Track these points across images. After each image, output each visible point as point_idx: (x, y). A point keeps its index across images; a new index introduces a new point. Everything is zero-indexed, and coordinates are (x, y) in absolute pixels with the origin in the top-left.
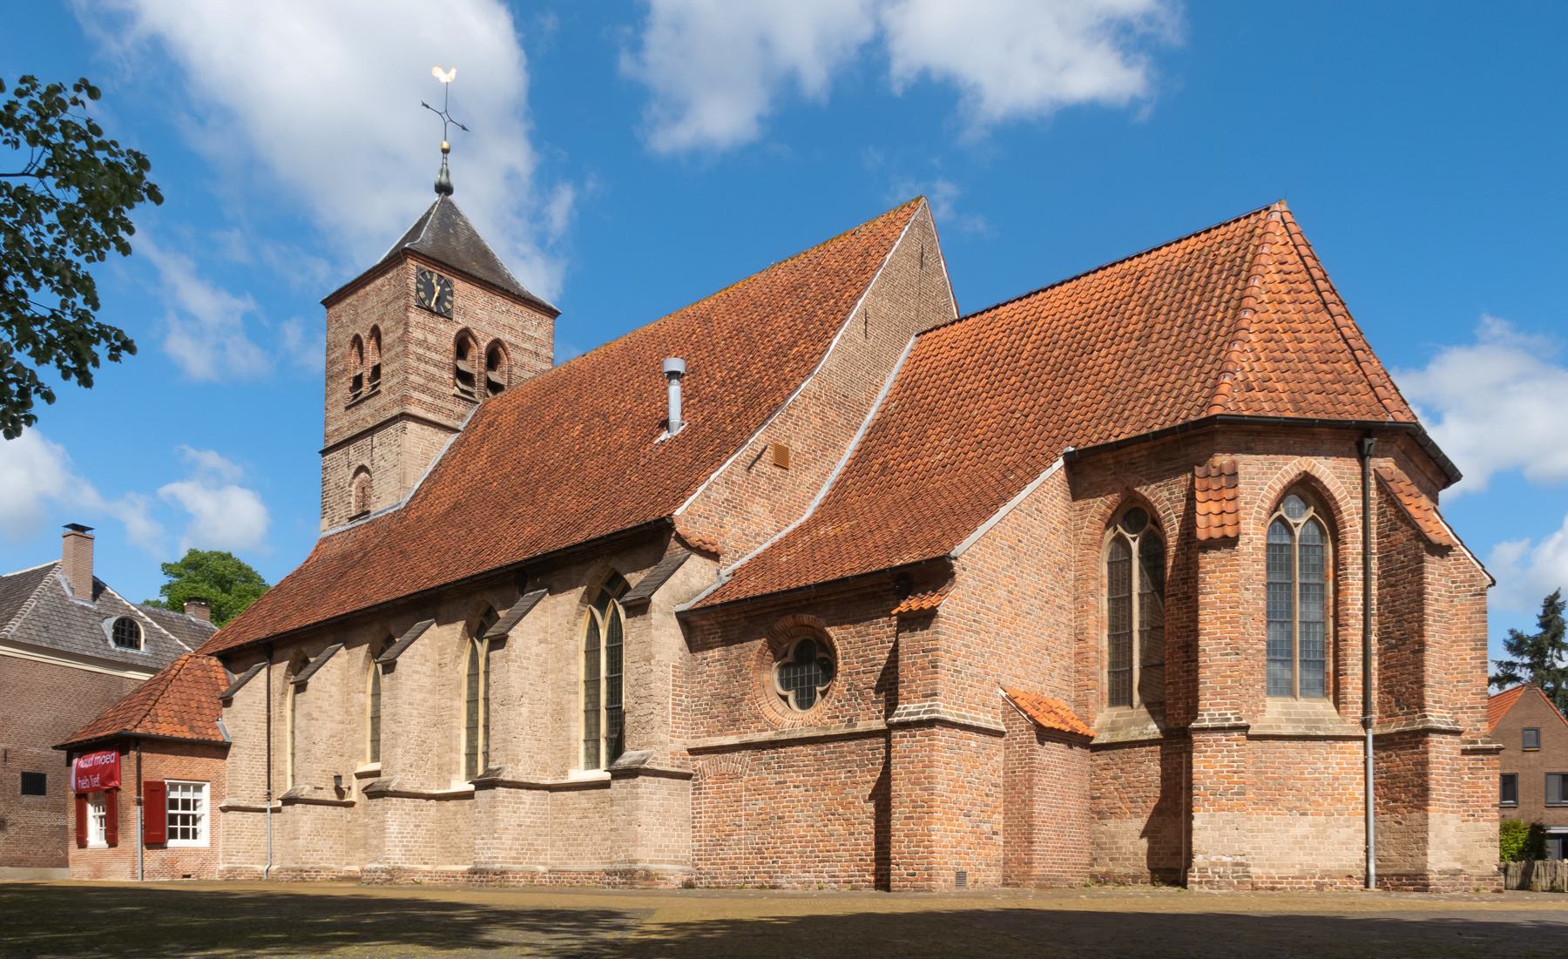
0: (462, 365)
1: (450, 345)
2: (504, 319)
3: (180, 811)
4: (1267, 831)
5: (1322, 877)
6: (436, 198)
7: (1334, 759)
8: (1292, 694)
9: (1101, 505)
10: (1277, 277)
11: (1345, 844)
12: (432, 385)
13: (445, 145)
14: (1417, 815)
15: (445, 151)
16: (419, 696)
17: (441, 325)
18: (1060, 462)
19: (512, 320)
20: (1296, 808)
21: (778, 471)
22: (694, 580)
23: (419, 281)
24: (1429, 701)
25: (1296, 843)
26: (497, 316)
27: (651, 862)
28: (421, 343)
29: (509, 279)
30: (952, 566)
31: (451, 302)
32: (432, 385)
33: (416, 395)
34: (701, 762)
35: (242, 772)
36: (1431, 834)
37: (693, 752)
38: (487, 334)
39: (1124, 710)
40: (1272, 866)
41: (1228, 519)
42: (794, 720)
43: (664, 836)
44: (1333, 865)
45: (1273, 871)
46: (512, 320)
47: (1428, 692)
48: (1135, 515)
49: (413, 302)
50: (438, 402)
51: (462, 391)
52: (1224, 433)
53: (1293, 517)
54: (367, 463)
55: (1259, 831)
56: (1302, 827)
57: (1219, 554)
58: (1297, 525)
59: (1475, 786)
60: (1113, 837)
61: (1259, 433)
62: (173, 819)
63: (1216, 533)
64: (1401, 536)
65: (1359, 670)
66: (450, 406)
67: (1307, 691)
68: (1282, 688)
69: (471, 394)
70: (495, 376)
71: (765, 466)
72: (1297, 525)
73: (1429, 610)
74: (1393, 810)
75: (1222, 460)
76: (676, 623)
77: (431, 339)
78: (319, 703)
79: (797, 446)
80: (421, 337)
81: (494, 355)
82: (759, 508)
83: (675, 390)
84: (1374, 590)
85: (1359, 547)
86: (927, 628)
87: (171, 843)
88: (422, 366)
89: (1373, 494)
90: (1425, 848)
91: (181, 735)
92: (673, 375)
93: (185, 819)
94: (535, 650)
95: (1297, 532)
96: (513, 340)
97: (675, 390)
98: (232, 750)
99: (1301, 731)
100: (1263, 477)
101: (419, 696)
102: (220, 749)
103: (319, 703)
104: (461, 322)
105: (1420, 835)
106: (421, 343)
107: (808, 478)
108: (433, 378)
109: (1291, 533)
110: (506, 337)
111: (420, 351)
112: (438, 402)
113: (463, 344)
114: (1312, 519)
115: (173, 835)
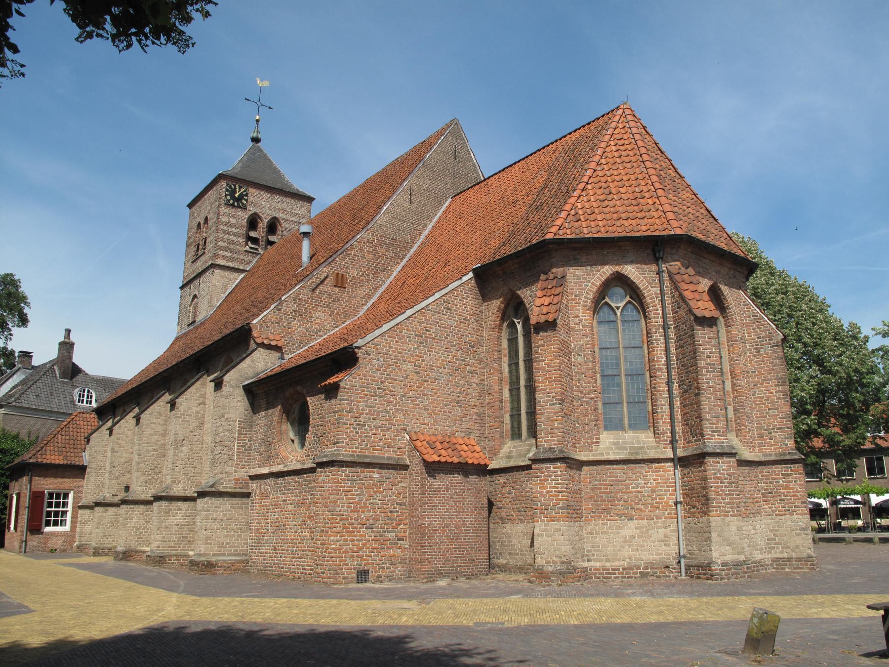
0: (253, 234)
1: (244, 223)
2: (279, 206)
3: (53, 509)
4: (603, 533)
5: (646, 568)
6: (251, 144)
7: (651, 476)
8: (622, 428)
9: (496, 304)
10: (614, 148)
11: (665, 541)
12: (232, 246)
13: (257, 117)
14: (704, 519)
15: (258, 121)
16: (154, 438)
17: (240, 213)
18: (471, 275)
19: (285, 206)
20: (624, 514)
21: (337, 290)
22: (258, 364)
23: (227, 190)
24: (708, 432)
25: (625, 542)
26: (274, 205)
27: (214, 555)
28: (226, 224)
29: (287, 184)
30: (355, 354)
31: (246, 200)
32: (232, 246)
33: (221, 253)
34: (254, 486)
35: (92, 487)
36: (714, 535)
37: (253, 478)
38: (268, 215)
39: (517, 442)
40: (608, 560)
41: (553, 308)
42: (293, 455)
43: (225, 536)
44: (654, 558)
45: (608, 564)
46: (285, 206)
47: (706, 424)
48: (515, 308)
49: (223, 202)
50: (235, 256)
51: (251, 248)
52: (556, 250)
53: (617, 303)
54: (197, 293)
55: (598, 533)
56: (630, 528)
57: (545, 334)
58: (618, 308)
59: (787, 487)
60: (509, 537)
61: (581, 249)
62: (49, 514)
63: (542, 319)
64: (682, 312)
65: (666, 409)
66: (242, 257)
67: (633, 427)
68: (614, 425)
69: (257, 249)
70: (271, 238)
71: (327, 287)
72: (618, 308)
73: (702, 364)
74: (693, 515)
75: (557, 271)
76: (243, 393)
77: (233, 221)
78: (119, 442)
79: (353, 272)
80: (227, 220)
81: (273, 226)
82: (320, 315)
83: (306, 244)
84: (673, 350)
85: (660, 321)
86: (336, 397)
87: (48, 529)
88: (226, 236)
89: (667, 283)
90: (709, 545)
91: (57, 462)
92: (306, 234)
93: (56, 514)
94: (195, 409)
95: (618, 312)
96: (284, 216)
97: (306, 244)
98: (88, 470)
99: (622, 456)
100: (584, 280)
101: (154, 438)
102: (79, 471)
103: (119, 442)
104: (252, 210)
105: (706, 535)
106: (226, 224)
107: (361, 292)
108: (232, 243)
109: (616, 314)
110: (280, 215)
111: (226, 228)
112: (235, 256)
113: (253, 222)
114: (629, 302)
115: (48, 524)
